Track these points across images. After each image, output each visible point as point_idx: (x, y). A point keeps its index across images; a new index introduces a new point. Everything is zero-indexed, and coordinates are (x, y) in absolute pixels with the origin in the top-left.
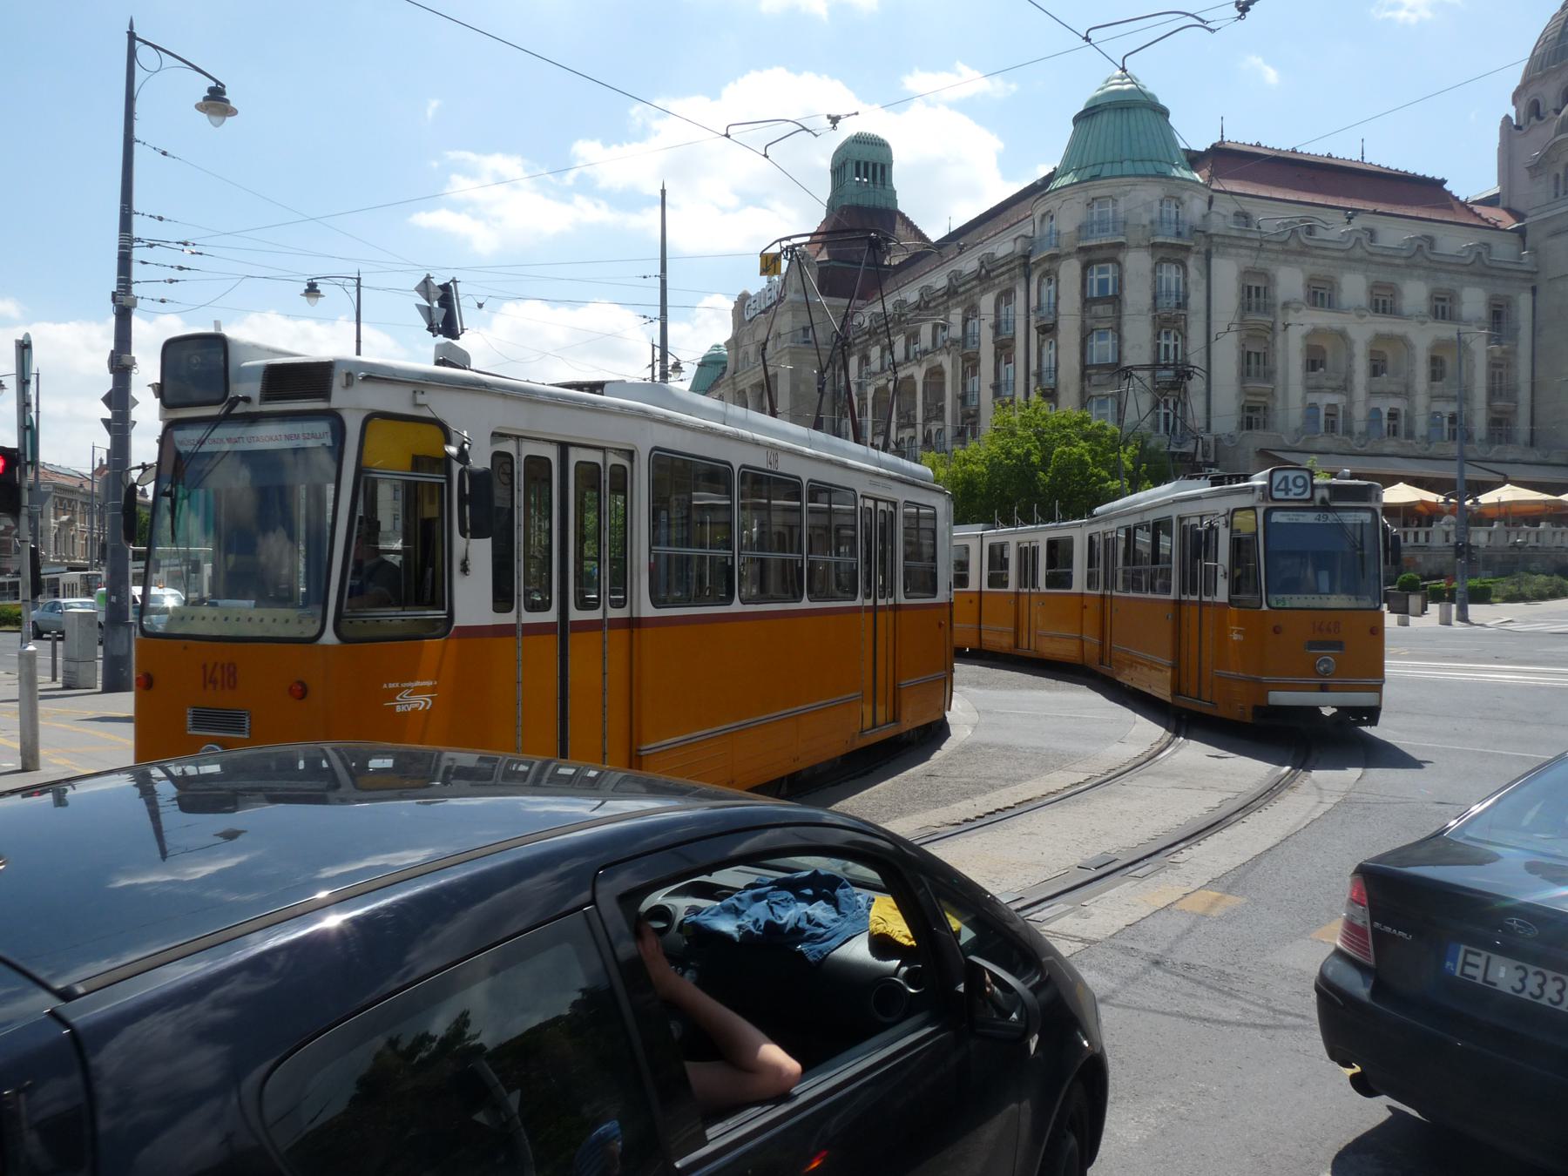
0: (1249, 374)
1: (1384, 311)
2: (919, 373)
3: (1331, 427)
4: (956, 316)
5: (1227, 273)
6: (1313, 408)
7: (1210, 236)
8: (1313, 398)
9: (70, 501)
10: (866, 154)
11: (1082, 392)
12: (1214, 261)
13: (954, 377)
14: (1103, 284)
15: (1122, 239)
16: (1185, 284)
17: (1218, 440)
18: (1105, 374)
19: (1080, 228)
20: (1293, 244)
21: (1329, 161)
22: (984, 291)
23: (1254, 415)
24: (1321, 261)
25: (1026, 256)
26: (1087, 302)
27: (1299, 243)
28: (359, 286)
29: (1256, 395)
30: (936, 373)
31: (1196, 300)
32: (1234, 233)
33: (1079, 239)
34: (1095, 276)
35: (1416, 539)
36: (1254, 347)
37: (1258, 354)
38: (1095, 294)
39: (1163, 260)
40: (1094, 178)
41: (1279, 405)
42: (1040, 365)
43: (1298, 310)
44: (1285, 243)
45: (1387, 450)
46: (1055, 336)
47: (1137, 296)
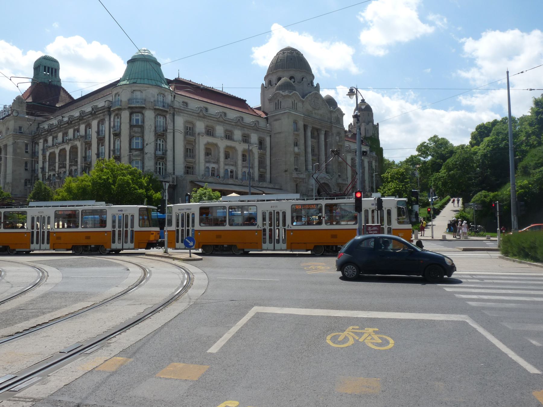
2: (68, 148)
5: (180, 122)
7: (174, 108)
10: (48, 64)
12: (175, 117)
13: (82, 149)
14: (137, 120)
15: (144, 106)
17: (177, 178)
19: (129, 100)
23: (189, 170)
26: (131, 126)
27: (222, 119)
30: (74, 149)
33: (129, 104)
36: (189, 147)
41: (197, 167)
42: (114, 147)
43: (203, 136)
44: (198, 113)
45: (230, 183)
46: (120, 137)
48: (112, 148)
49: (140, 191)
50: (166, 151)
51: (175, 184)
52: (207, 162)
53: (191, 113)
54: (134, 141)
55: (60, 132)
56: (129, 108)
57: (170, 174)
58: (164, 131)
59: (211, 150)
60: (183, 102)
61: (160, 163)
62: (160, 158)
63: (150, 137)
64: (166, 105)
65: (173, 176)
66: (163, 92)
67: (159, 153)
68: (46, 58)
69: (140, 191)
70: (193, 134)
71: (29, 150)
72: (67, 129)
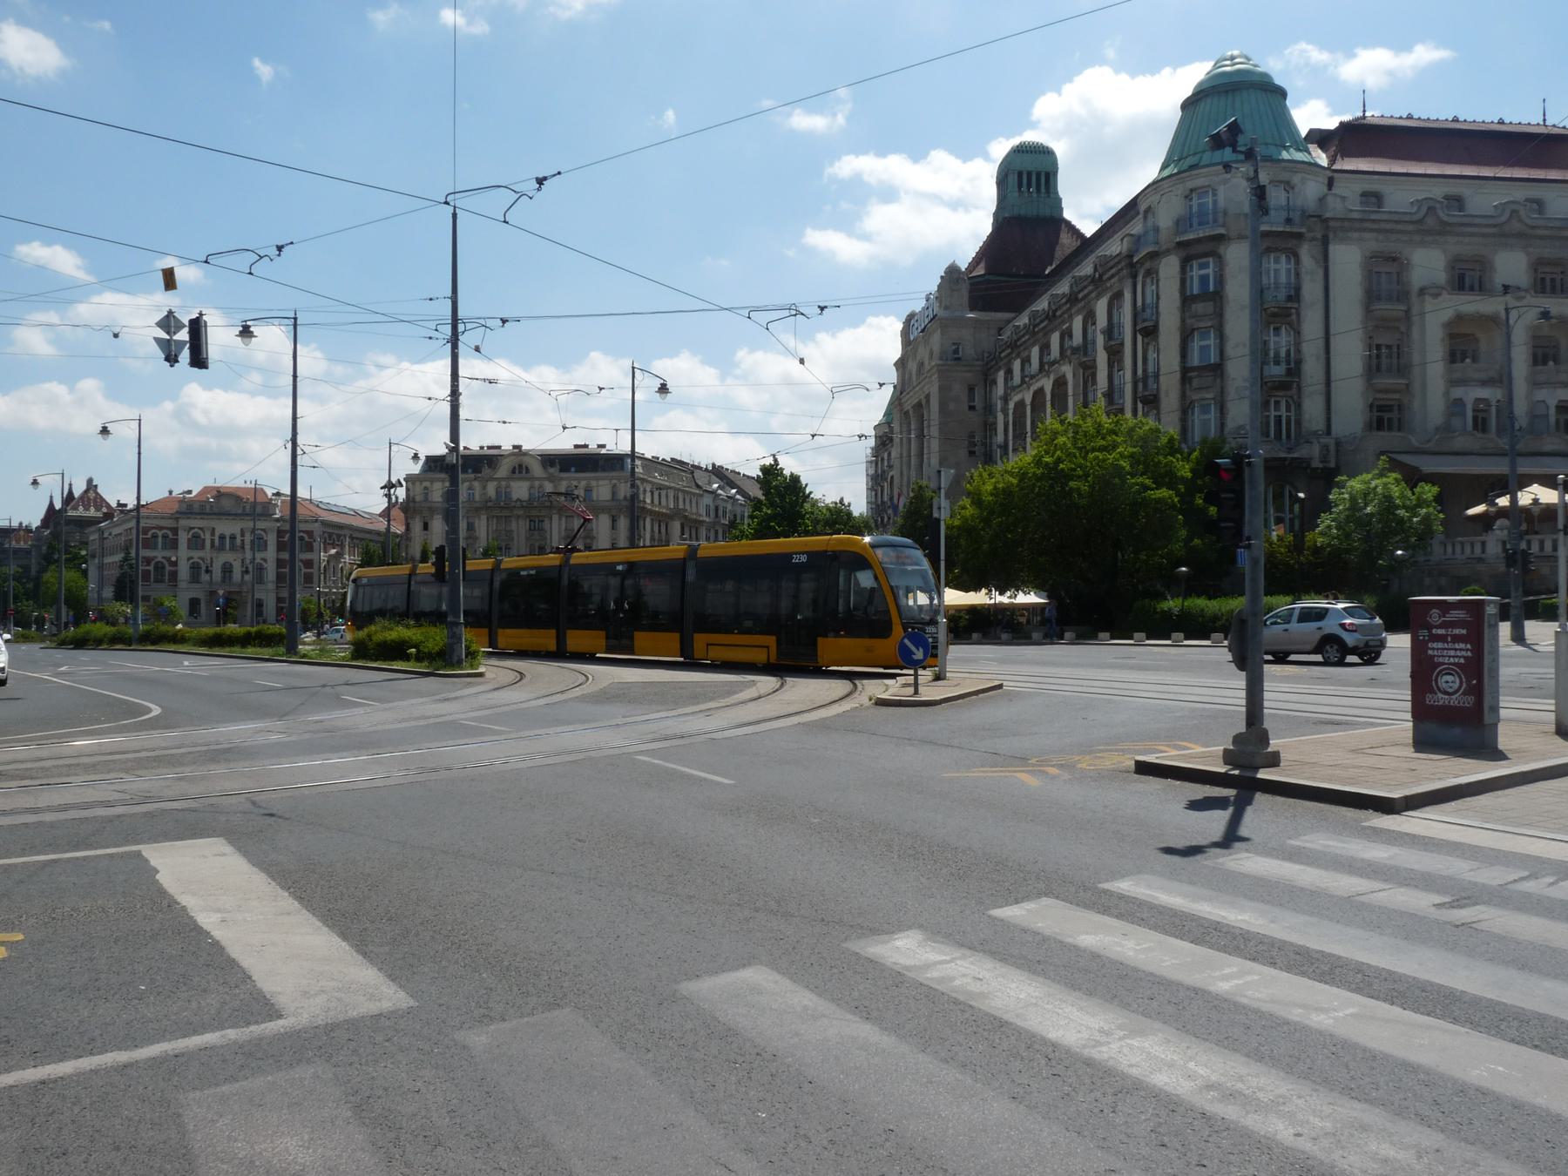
0: (1378, 369)
1: (1553, 290)
2: (1047, 384)
3: (1480, 424)
4: (1077, 323)
5: (1348, 259)
6: (1459, 403)
7: (1325, 221)
8: (1457, 393)
9: (339, 536)
10: (1029, 164)
11: (1183, 396)
12: (1332, 248)
13: (1075, 386)
14: (1204, 280)
15: (1222, 231)
16: (1298, 275)
17: (1338, 444)
18: (1203, 376)
19: (1177, 223)
20: (1431, 222)
21: (1457, 126)
22: (1098, 297)
23: (1386, 416)
24: (1467, 240)
25: (1130, 256)
26: (1187, 300)
27: (1434, 221)
28: (295, 326)
29: (1387, 391)
30: (1060, 383)
31: (1311, 290)
32: (1356, 216)
33: (1177, 233)
34: (1195, 273)
35: (1542, 548)
36: (1384, 339)
37: (1389, 347)
38: (1196, 291)
39: (1269, 250)
40: (1192, 167)
41: (1416, 405)
42: (1145, 370)
43: (1436, 296)
44: (1420, 222)
45: (1548, 448)
46: (1156, 339)
47: (1238, 290)
48: (1140, 372)
49: (1163, 493)
50: (1299, 362)
51: (1332, 465)
52: (1453, 383)
53: (1388, 226)
54: (1196, 344)
55: (1033, 345)
56: (1180, 245)
57: (1315, 433)
58: (1289, 298)
59: (1477, 340)
60: (1364, 194)
61: (1277, 403)
62: (1280, 385)
63: (1239, 325)
64: (1296, 216)
65: (1325, 440)
66: (1285, 176)
67: (1277, 371)
68: (1022, 151)
69: (1163, 493)
70: (1402, 295)
71: (978, 403)
72: (1047, 333)
